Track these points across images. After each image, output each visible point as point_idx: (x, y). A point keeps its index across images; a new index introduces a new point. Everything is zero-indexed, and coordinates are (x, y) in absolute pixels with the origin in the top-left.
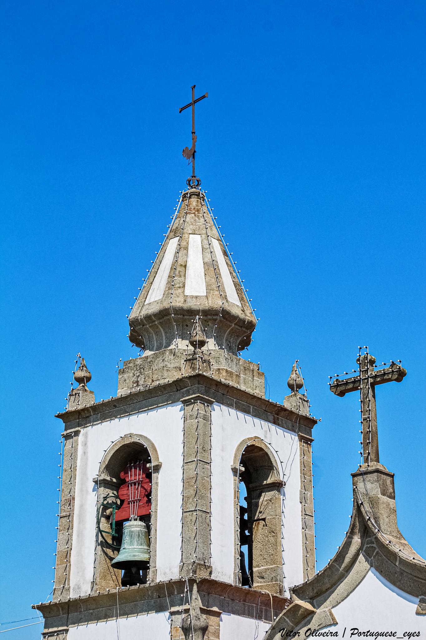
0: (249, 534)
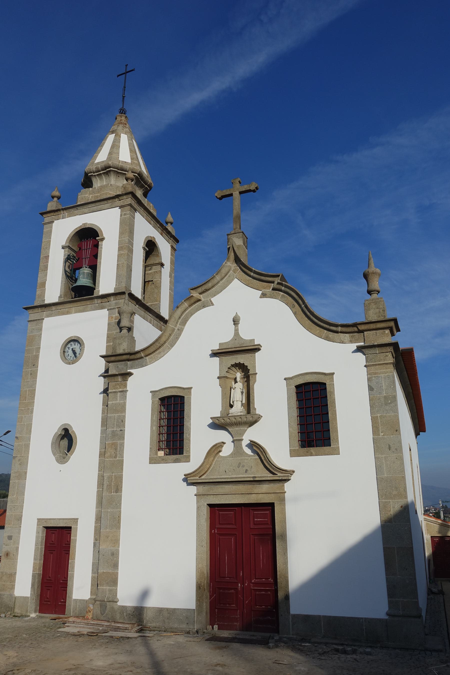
0: (169, 213)
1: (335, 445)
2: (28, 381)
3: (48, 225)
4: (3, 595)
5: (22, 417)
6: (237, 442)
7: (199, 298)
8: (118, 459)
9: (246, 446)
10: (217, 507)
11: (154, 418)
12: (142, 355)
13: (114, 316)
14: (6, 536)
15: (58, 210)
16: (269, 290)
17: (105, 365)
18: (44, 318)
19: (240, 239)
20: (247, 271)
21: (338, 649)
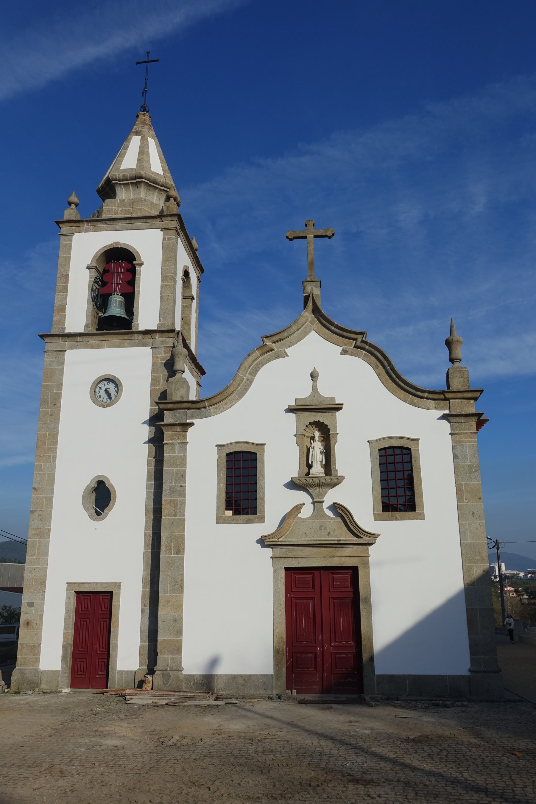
1: (420, 510)
2: (47, 423)
3: (66, 237)
4: (25, 670)
5: (42, 466)
6: (317, 504)
7: (273, 348)
8: (178, 517)
9: (327, 508)
10: (293, 571)
11: (221, 475)
12: (207, 404)
13: (160, 356)
14: (24, 602)
15: (81, 221)
16: (350, 347)
17: (150, 412)
18: (65, 349)
19: (317, 289)
20: (327, 324)
21: (439, 704)
